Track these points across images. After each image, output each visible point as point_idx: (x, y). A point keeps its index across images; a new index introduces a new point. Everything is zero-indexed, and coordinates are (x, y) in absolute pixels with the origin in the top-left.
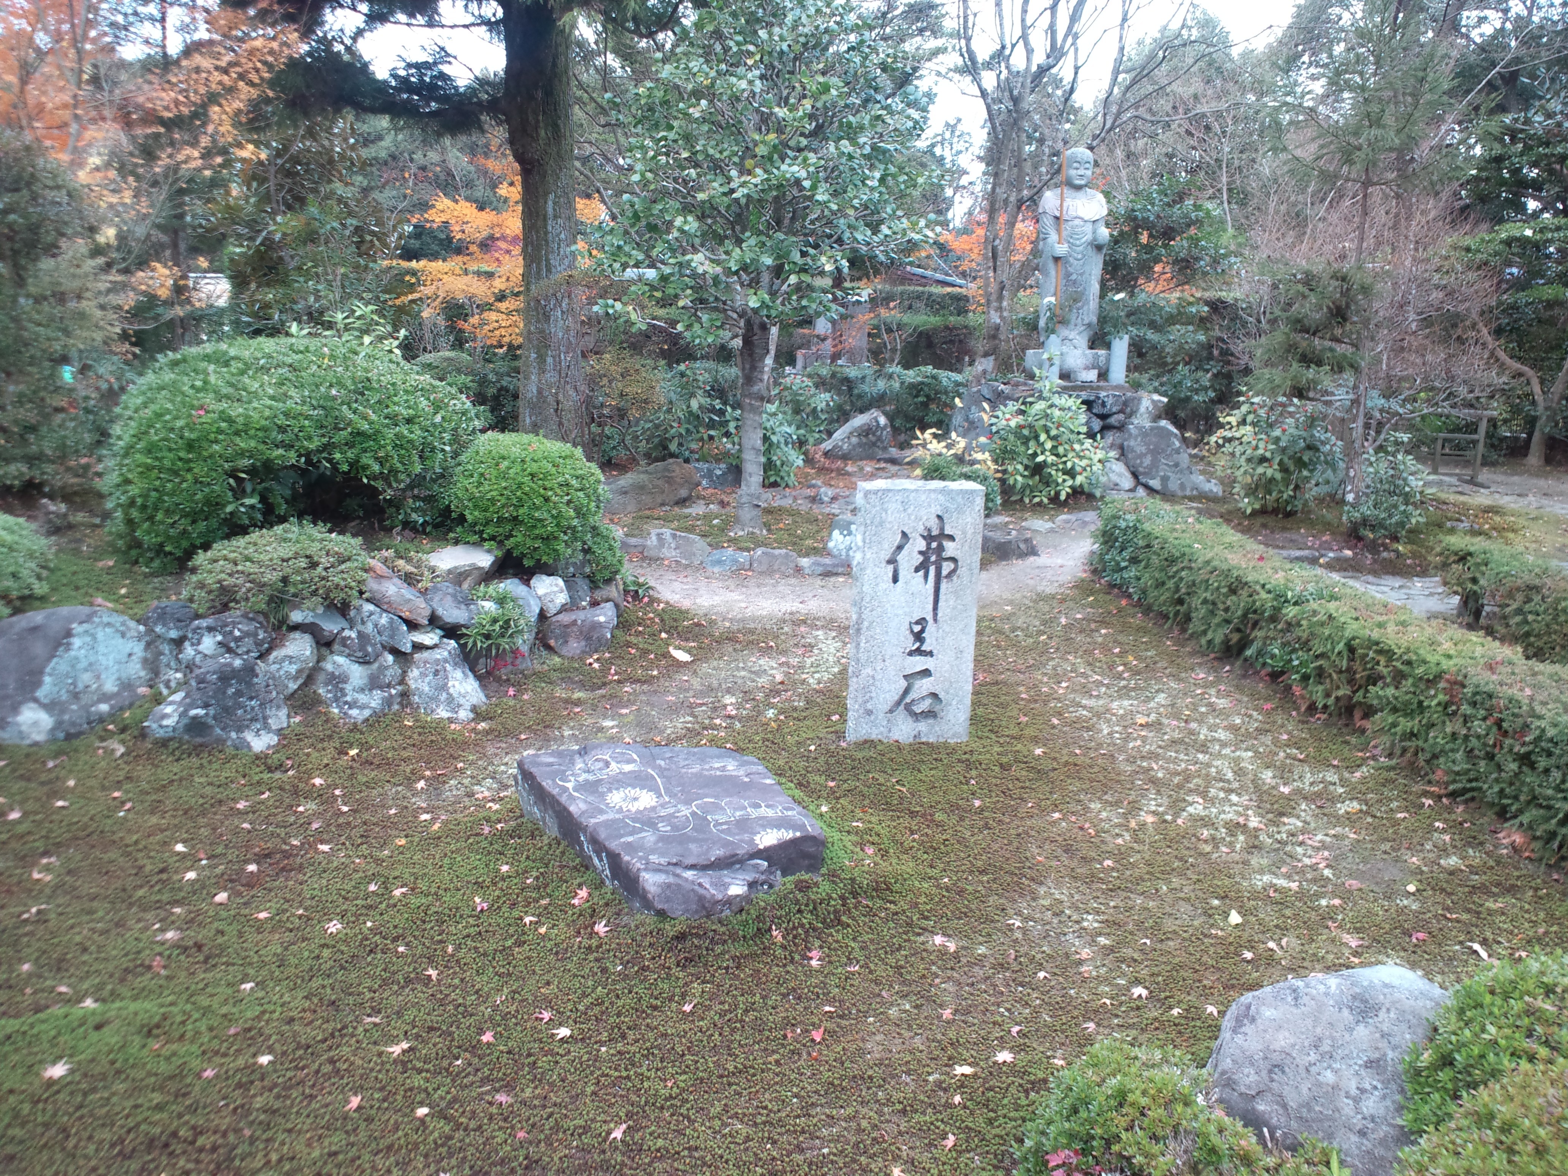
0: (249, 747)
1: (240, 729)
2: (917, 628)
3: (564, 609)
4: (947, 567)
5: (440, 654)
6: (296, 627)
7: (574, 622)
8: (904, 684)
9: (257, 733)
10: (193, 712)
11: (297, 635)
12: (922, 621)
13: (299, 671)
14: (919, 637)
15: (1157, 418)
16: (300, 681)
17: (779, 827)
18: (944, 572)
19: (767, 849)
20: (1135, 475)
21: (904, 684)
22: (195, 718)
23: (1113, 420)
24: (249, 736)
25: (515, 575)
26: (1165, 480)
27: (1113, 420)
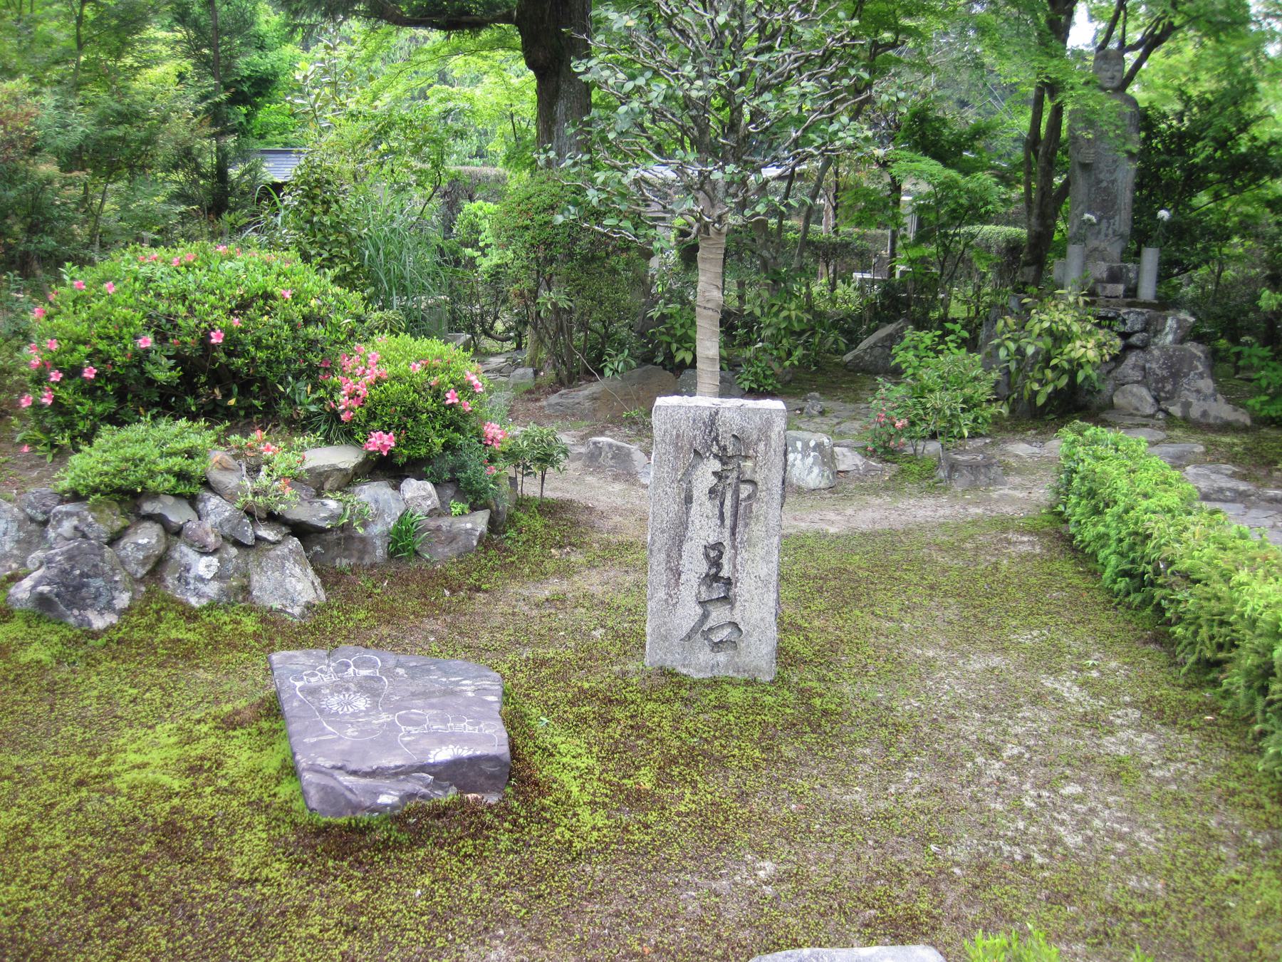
0: (90, 624)
1: (84, 607)
2: (713, 554)
3: (431, 513)
4: (745, 490)
5: (280, 550)
6: (150, 517)
7: (438, 529)
8: (699, 611)
9: (101, 613)
10: (40, 588)
11: (147, 524)
12: (718, 546)
13: (147, 558)
14: (716, 563)
15: (1181, 341)
16: (148, 567)
17: (455, 743)
18: (742, 496)
19: (434, 765)
20: (1157, 400)
21: (699, 611)
22: (41, 594)
23: (1134, 340)
24: (91, 615)
25: (384, 478)
26: (1187, 405)
27: (1134, 340)
